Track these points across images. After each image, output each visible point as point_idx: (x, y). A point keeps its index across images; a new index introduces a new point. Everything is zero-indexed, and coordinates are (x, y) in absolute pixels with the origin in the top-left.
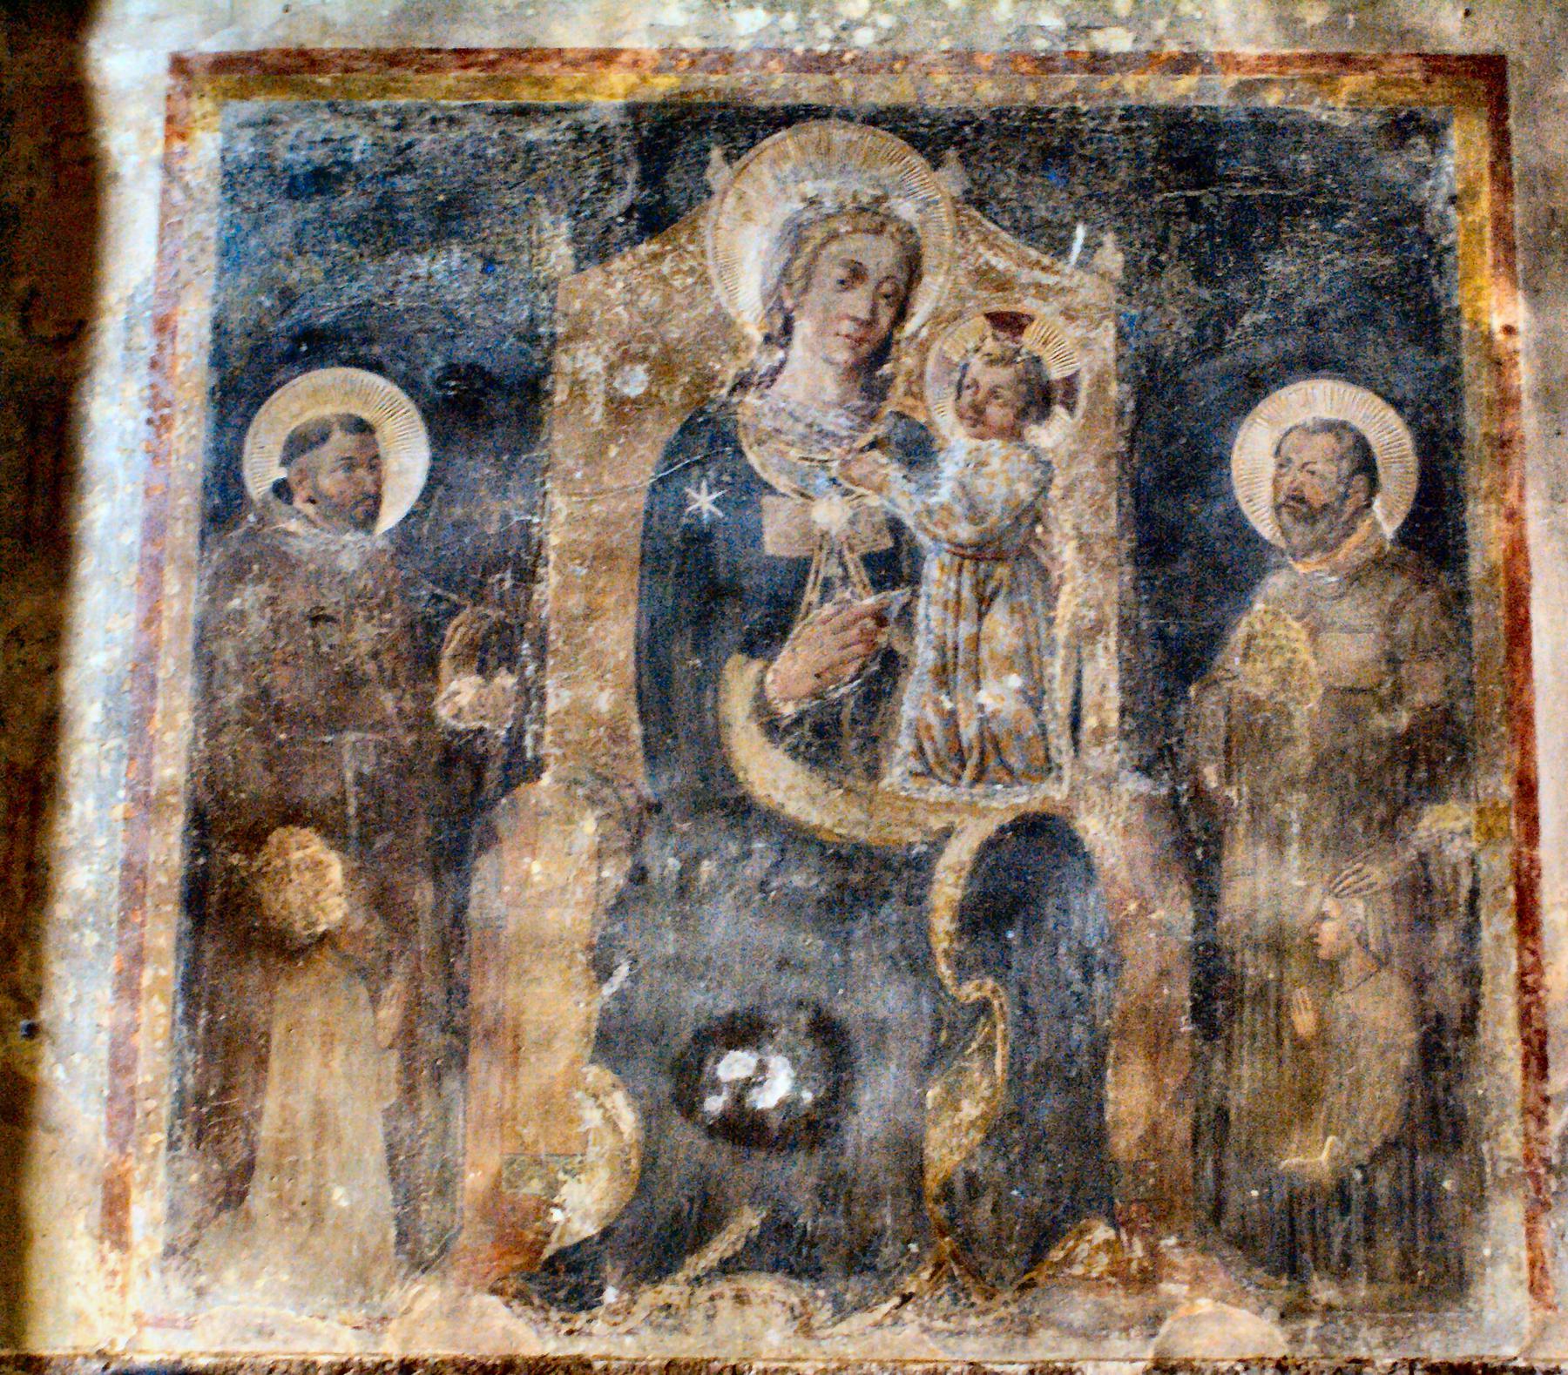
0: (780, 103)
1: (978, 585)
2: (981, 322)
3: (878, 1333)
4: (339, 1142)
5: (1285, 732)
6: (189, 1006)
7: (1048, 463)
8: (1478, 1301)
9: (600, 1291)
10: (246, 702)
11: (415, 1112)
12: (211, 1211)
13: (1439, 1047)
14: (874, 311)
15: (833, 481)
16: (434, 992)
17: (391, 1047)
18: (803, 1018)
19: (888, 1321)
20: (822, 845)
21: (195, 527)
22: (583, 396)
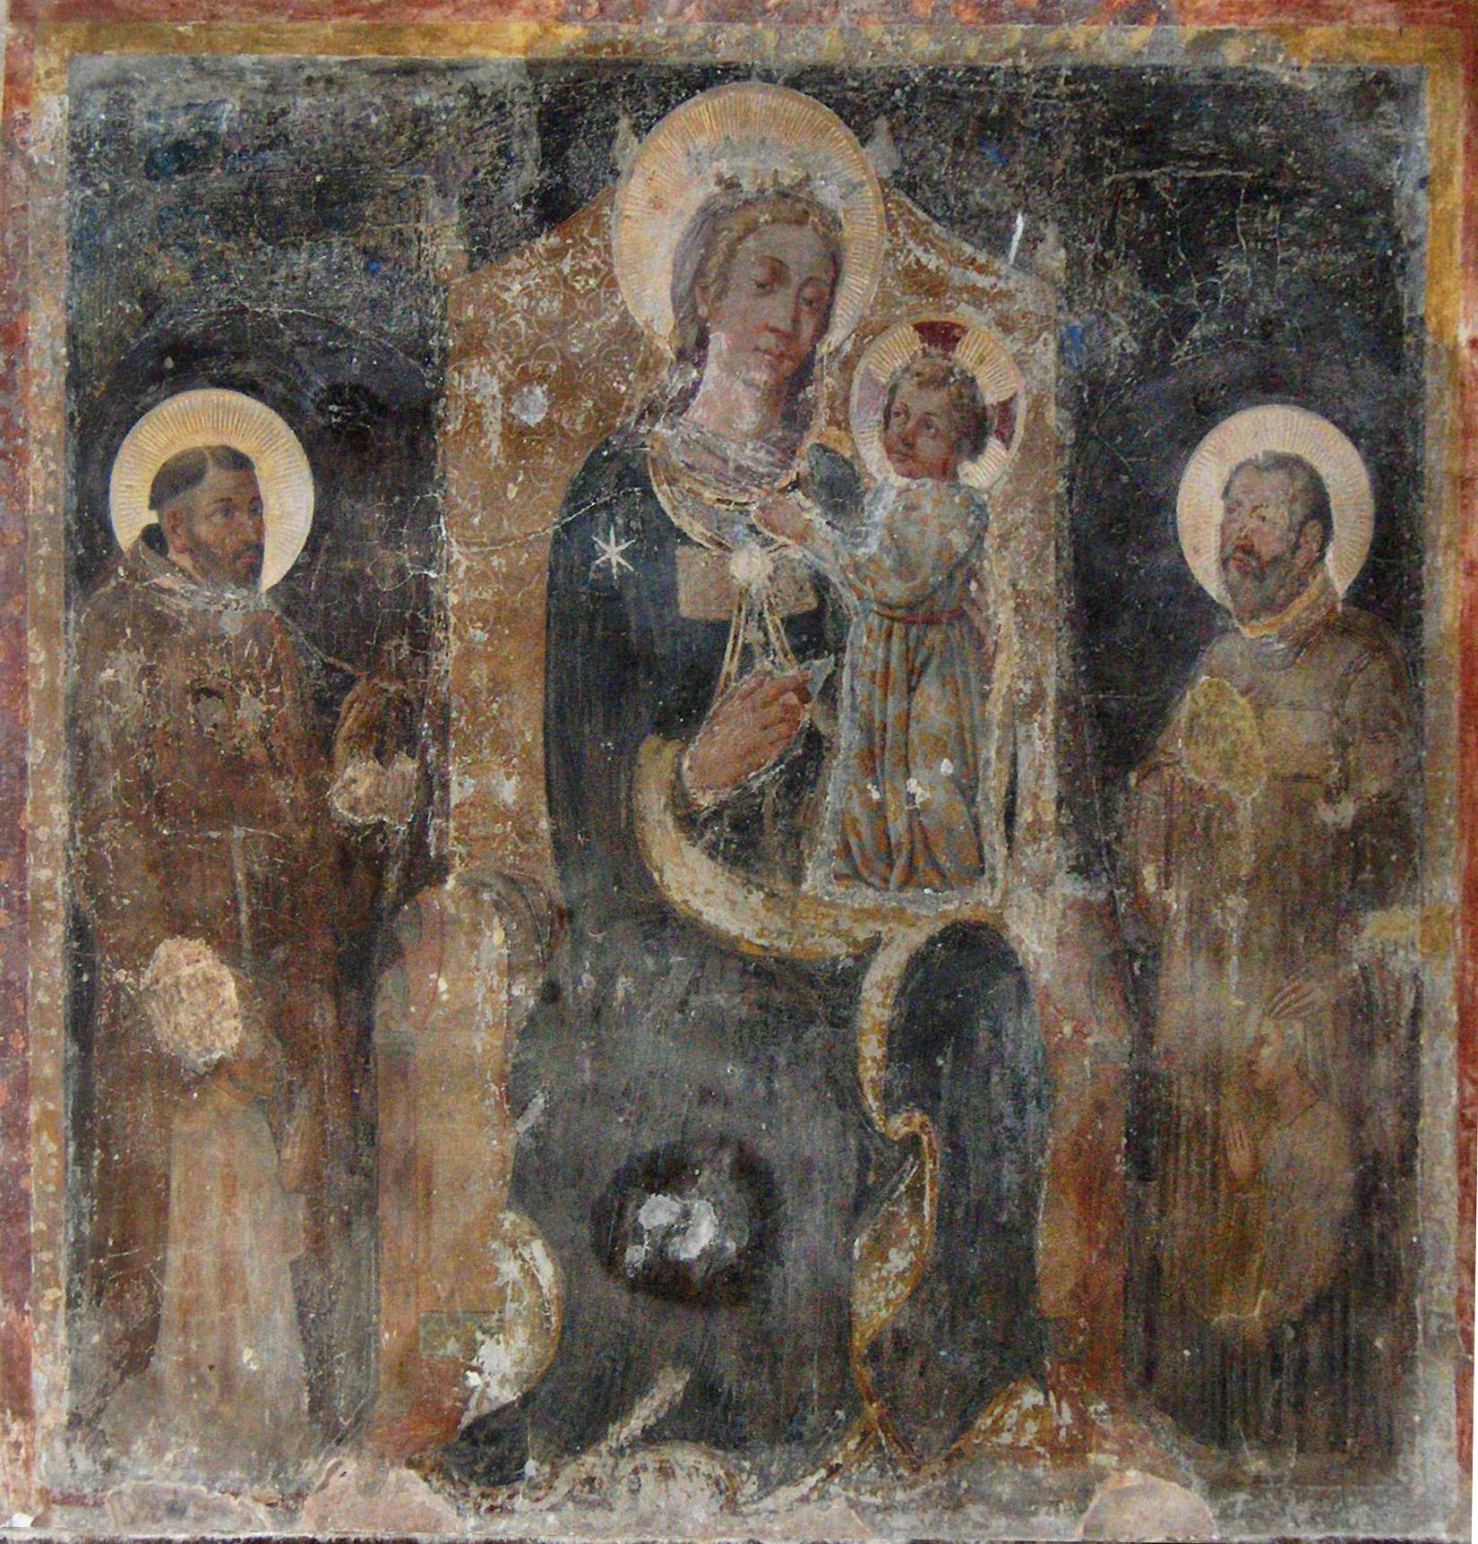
0: (697, 61)
1: (907, 654)
2: (908, 332)
3: (806, 1509)
4: (246, 1298)
5: (1227, 827)
6: (80, 1146)
7: (982, 507)
8: (1406, 1470)
9: (522, 1464)
10: (126, 791)
11: (324, 1264)
12: (116, 1376)
13: (1376, 1189)
14: (796, 321)
15: (752, 527)
16: (336, 1124)
17: (297, 1190)
18: (727, 1158)
19: (815, 1496)
20: (743, 958)
21: (59, 583)
22: (479, 424)
